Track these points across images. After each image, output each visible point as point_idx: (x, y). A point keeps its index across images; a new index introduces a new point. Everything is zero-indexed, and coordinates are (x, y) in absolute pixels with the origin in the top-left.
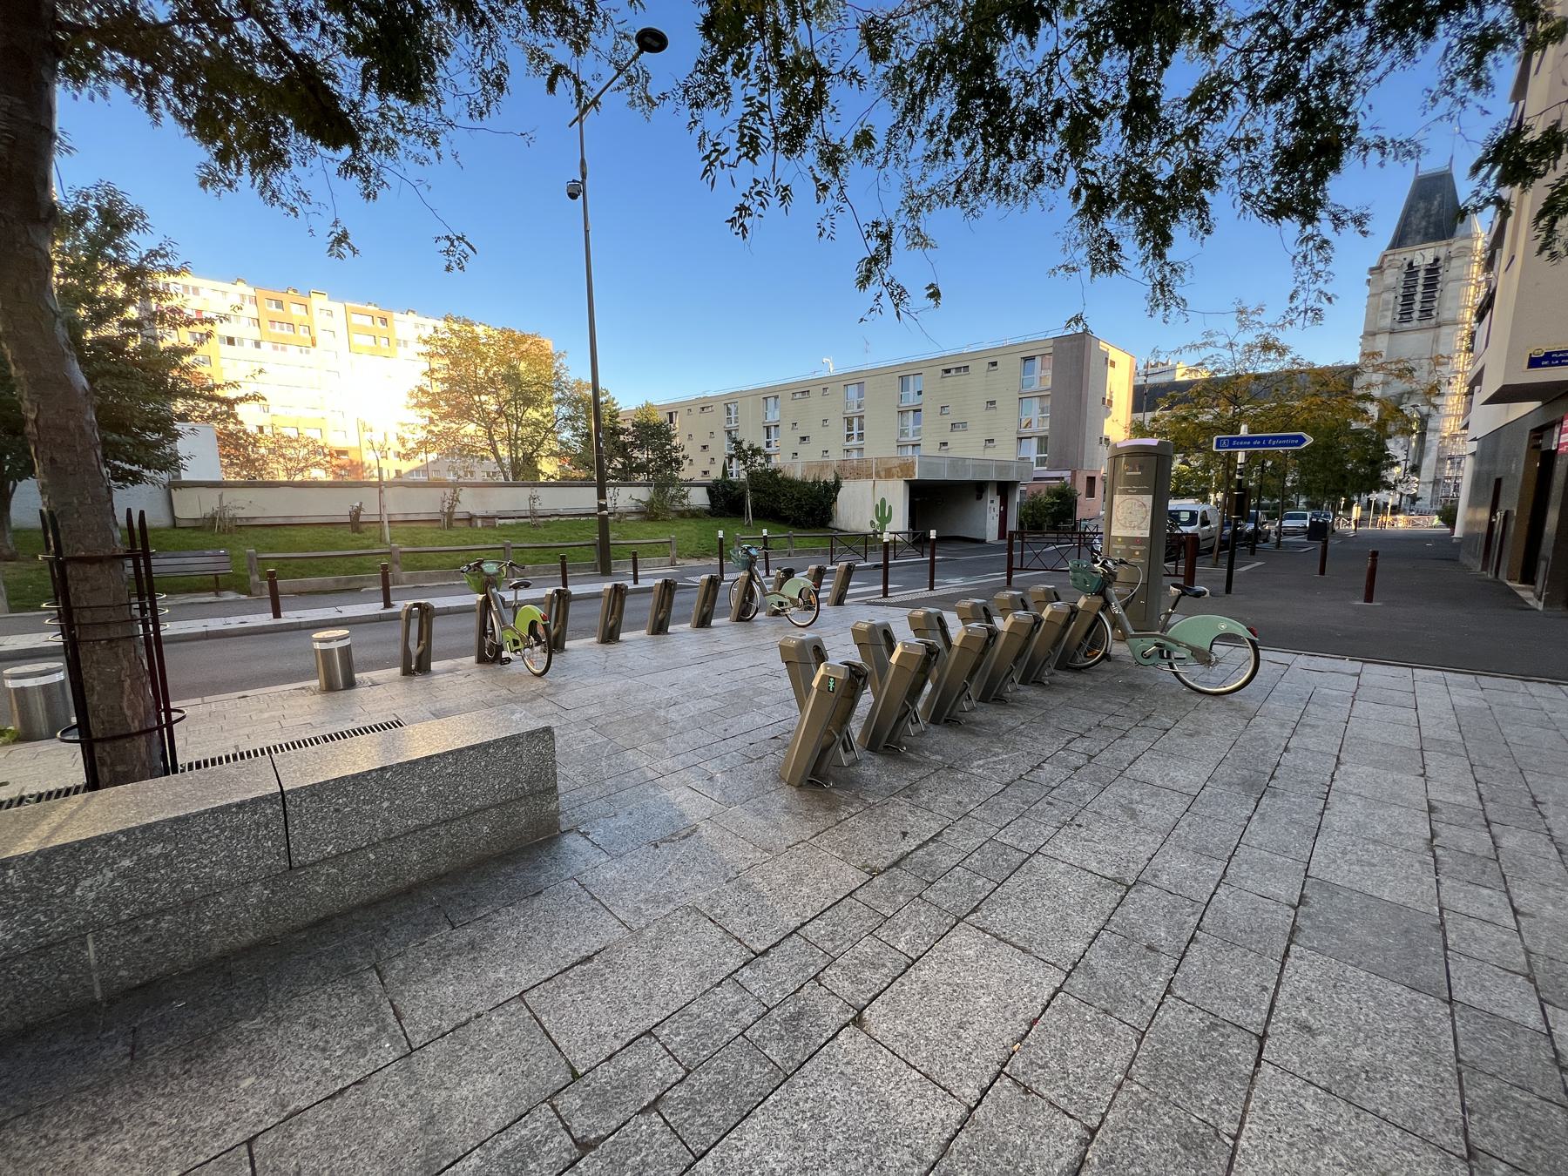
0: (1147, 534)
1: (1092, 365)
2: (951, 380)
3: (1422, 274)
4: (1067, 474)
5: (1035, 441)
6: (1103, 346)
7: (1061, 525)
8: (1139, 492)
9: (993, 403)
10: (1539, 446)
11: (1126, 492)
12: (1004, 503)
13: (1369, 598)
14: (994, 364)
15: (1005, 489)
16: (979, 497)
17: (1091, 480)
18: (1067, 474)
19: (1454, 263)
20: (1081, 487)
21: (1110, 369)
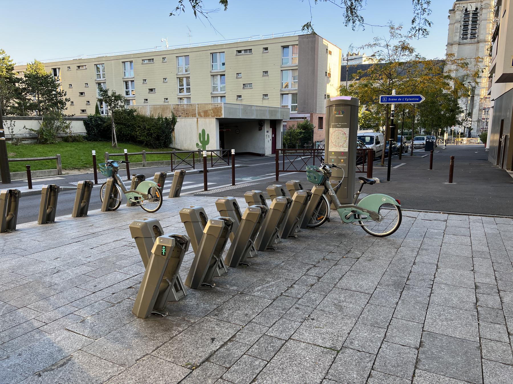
0: (347, 150)
2: (243, 57)
3: (471, 15)
4: (307, 115)
5: (290, 96)
6: (325, 42)
8: (343, 127)
9: (266, 72)
12: (274, 132)
13: (451, 181)
14: (266, 49)
15: (274, 124)
16: (260, 129)
18: (307, 115)
19: (484, 10)
21: (329, 55)
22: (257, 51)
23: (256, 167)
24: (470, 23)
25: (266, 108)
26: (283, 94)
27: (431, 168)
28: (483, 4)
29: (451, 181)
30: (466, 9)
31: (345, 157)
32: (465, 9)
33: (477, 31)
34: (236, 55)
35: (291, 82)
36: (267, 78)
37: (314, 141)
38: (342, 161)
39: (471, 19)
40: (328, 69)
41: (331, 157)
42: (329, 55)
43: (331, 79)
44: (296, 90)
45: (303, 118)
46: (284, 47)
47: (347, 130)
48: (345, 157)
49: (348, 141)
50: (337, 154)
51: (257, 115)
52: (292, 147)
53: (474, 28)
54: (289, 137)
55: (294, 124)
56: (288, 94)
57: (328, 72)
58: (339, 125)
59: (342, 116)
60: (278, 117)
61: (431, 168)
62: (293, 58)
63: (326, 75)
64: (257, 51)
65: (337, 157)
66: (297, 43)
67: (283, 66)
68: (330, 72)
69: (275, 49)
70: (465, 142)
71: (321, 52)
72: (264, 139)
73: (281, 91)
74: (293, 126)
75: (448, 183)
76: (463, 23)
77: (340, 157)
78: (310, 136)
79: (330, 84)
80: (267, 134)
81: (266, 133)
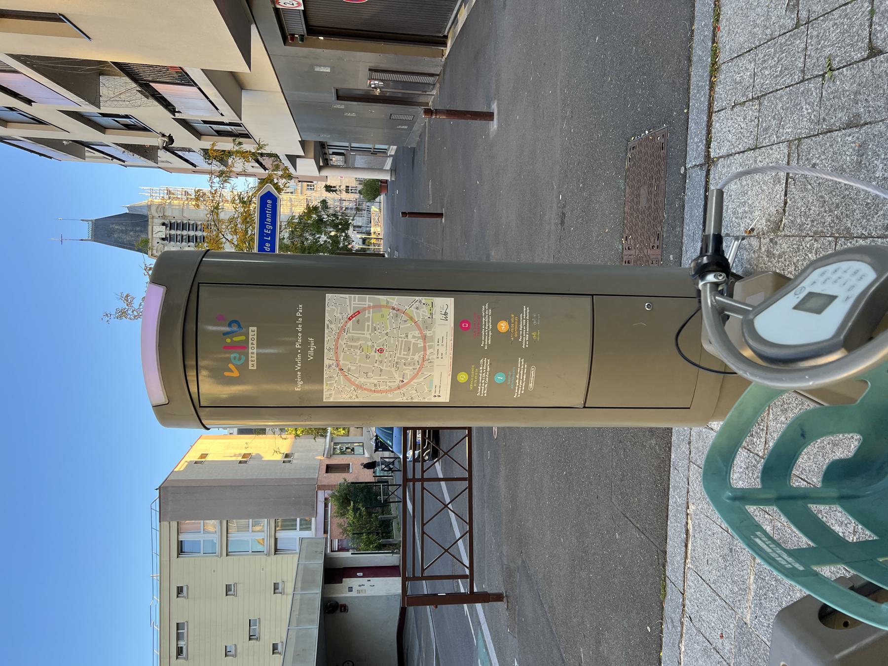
0: (445, 304)
1: (206, 477)
2: (191, 644)
3: (173, 232)
4: (321, 496)
5: (281, 534)
6: (181, 467)
7: (382, 498)
8: (316, 325)
9: (228, 588)
10: (302, 38)
11: (315, 370)
12: (351, 572)
13: (489, 116)
14: (180, 590)
15: (334, 573)
16: (344, 608)
17: (329, 469)
18: (321, 496)
19: (167, 214)
20: (337, 478)
21: (208, 458)
22: (182, 610)
23: (437, 626)
24: (185, 233)
25: (298, 597)
26: (276, 550)
27: (440, 215)
28: (157, 215)
29: (489, 116)
30: (163, 239)
31: (486, 311)
32: (161, 241)
33: (199, 223)
34: (187, 658)
35: (254, 534)
36: (240, 588)
37: (372, 480)
38: (503, 326)
39: (179, 232)
40: (234, 459)
41: (483, 390)
42: (208, 458)
43: (253, 451)
44: (269, 523)
45: (326, 506)
46: (181, 551)
47: (338, 306)
48: (486, 311)
49: (395, 300)
50: (464, 356)
51: (311, 622)
52: (385, 528)
53: (196, 227)
54: (364, 536)
55: (338, 523)
56: (276, 539)
57: (240, 459)
58: (306, 344)
59: (253, 331)
60: (318, 565)
61: (440, 215)
62: (207, 531)
63: (246, 462)
64: (182, 610)
65: (485, 354)
66: (174, 524)
67: (218, 550)
68: (240, 455)
69: (184, 570)
70: (379, 230)
71: (200, 475)
72: (367, 597)
73: (268, 554)
74: (340, 526)
75: (494, 125)
76: (184, 243)
77: (487, 340)
78: (362, 490)
79: (262, 454)
80: (357, 589)
81: (354, 594)
